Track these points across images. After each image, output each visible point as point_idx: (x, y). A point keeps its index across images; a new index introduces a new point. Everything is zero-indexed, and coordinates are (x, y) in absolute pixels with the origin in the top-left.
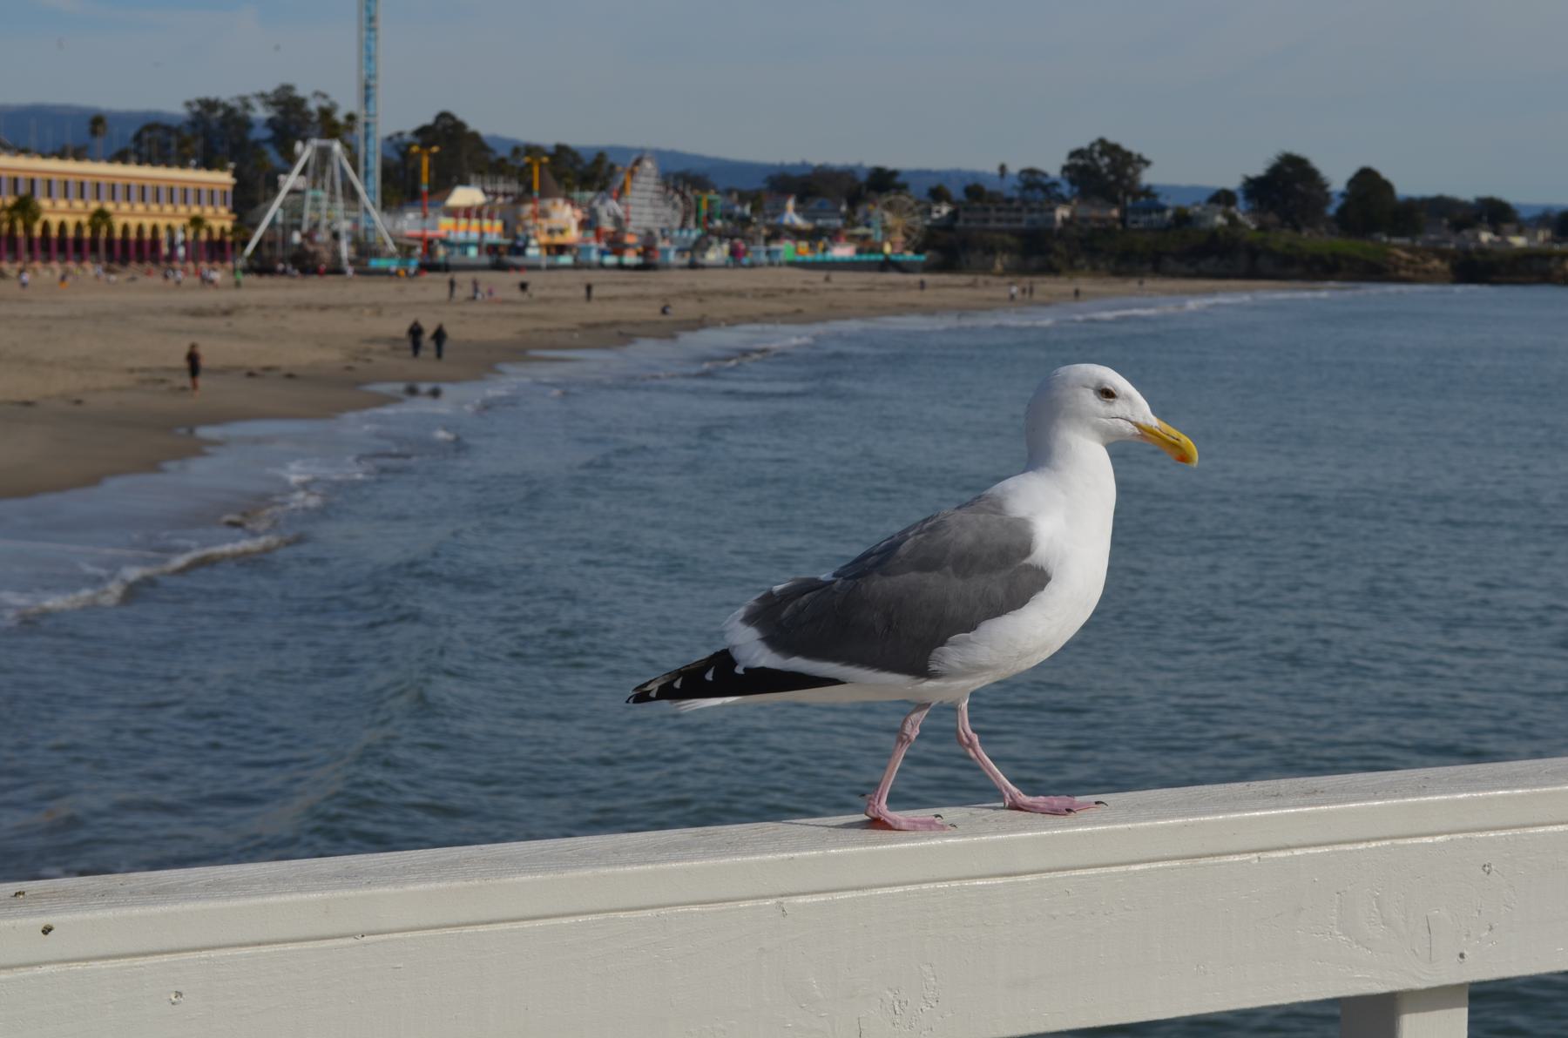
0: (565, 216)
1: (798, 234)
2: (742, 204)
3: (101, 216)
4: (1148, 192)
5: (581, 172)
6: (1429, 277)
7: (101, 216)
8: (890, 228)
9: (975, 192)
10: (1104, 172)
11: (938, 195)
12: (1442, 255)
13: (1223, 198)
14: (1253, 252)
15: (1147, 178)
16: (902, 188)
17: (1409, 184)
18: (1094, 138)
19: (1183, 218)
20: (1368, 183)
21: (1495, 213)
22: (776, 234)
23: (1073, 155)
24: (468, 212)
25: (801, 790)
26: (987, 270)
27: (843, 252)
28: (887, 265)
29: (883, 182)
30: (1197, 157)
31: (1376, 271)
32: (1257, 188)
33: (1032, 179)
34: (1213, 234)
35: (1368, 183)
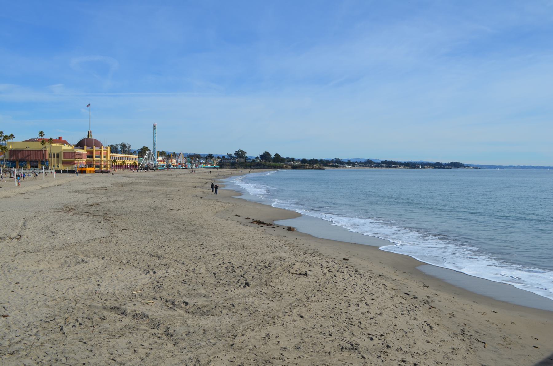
0: (174, 161)
1: (204, 163)
2: (194, 158)
3: (124, 162)
4: (247, 157)
5: (175, 155)
6: (288, 169)
7: (124, 162)
8: (215, 162)
9: (223, 157)
10: (240, 154)
11: (218, 158)
12: (290, 165)
13: (257, 158)
14: (264, 165)
15: (246, 155)
16: (213, 157)
17: (283, 155)
18: (173, 152)
19: (254, 161)
20: (277, 155)
21: (293, 160)
22: (201, 163)
23: (241, 151)
24: (160, 161)
25: (93, 207)
26: (226, 168)
27: (209, 166)
28: (215, 168)
29: (210, 156)
30: (253, 153)
31: (281, 168)
32: (262, 156)
33: (230, 156)
34: (258, 163)
35: (277, 155)
